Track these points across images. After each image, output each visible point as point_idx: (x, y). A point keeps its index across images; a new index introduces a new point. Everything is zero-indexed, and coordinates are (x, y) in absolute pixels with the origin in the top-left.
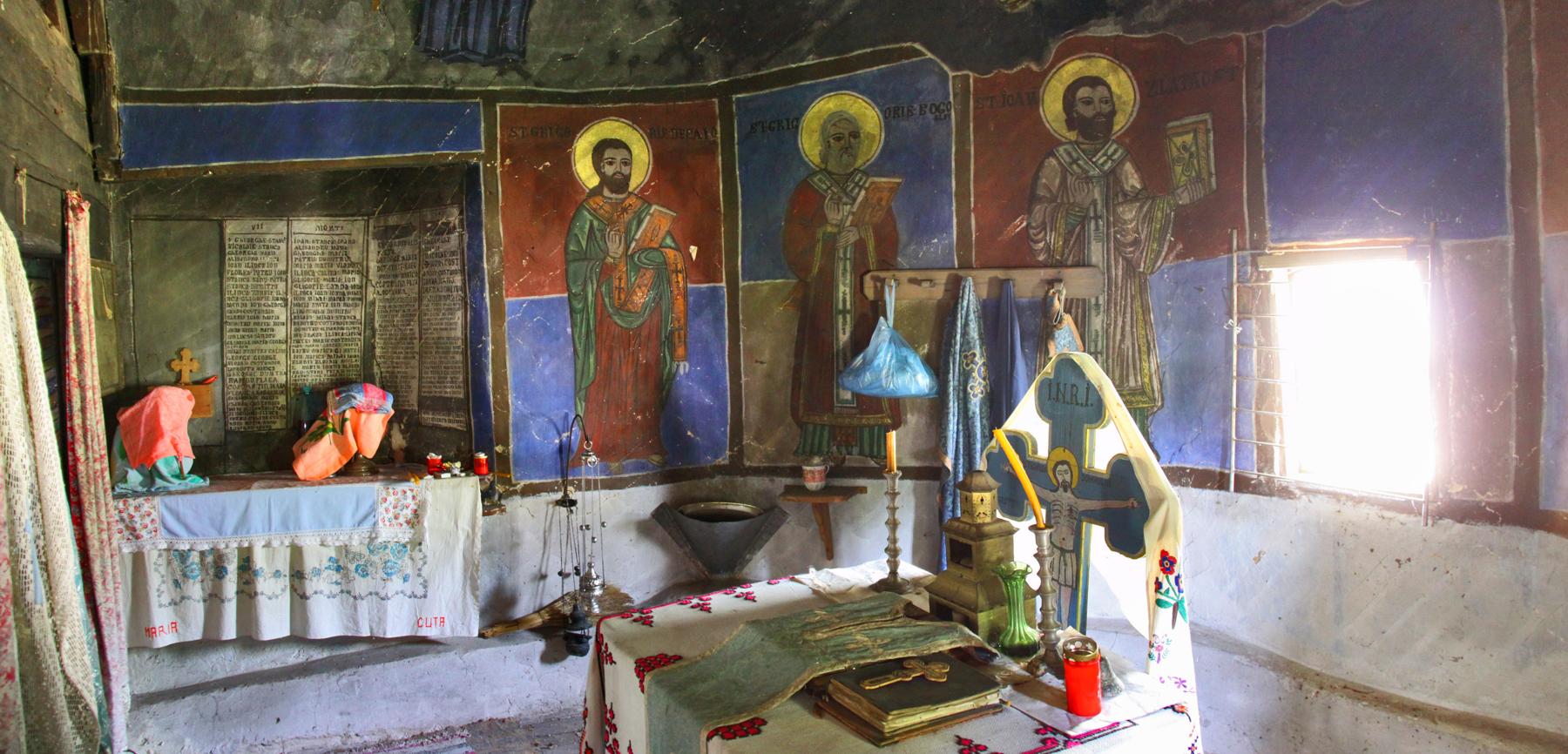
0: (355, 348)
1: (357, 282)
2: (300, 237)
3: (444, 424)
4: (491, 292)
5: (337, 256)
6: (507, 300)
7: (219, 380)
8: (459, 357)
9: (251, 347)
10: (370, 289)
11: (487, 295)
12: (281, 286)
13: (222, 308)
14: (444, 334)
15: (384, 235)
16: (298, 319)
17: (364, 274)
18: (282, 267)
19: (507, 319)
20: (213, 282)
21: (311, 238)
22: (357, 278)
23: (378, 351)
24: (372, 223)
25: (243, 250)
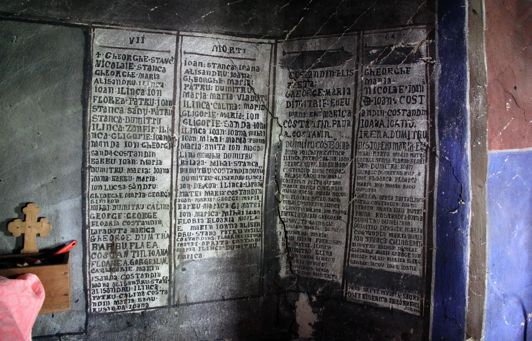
0: (256, 204)
1: (261, 120)
2: (193, 58)
3: (382, 304)
4: (473, 141)
5: (238, 83)
6: (489, 152)
7: (79, 246)
8: (417, 224)
9: (124, 201)
10: (276, 129)
11: (468, 145)
12: (166, 120)
13: (84, 147)
14: (394, 192)
15: (298, 64)
16: (185, 166)
17: (270, 110)
18: (167, 95)
19: (489, 176)
20: (73, 111)
21: (205, 60)
22: (262, 114)
23: (283, 207)
24: (280, 48)
25: (116, 70)
